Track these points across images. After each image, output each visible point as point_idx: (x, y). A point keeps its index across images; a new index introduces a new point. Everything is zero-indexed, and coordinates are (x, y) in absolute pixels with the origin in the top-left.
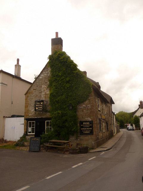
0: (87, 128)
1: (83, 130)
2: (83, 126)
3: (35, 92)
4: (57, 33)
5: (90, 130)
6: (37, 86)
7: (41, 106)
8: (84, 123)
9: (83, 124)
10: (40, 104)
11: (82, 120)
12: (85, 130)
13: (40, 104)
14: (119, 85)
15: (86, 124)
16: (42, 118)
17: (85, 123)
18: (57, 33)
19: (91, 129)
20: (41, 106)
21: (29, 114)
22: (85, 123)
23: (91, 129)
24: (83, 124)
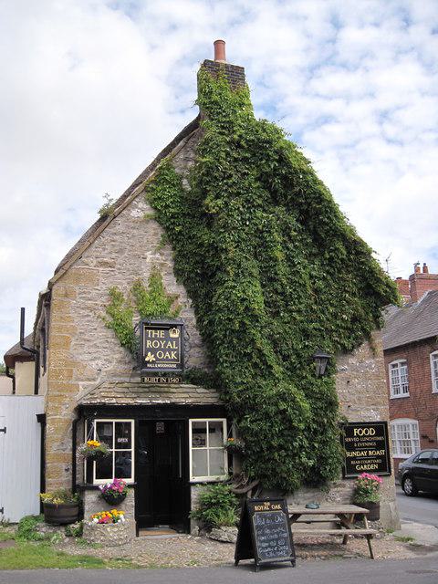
0: (367, 449)
1: (354, 458)
2: (352, 443)
3: (107, 276)
4: (219, 45)
5: (378, 457)
6: (121, 251)
7: (170, 350)
8: (356, 431)
9: (353, 436)
10: (168, 338)
11: (352, 419)
12: (362, 459)
13: (168, 338)
14: (68, 230)
15: (364, 436)
16: (174, 407)
17: (361, 432)
18: (219, 45)
19: (381, 452)
20: (170, 350)
21: (78, 379)
22: (361, 432)
23: (381, 452)
24: (353, 436)
